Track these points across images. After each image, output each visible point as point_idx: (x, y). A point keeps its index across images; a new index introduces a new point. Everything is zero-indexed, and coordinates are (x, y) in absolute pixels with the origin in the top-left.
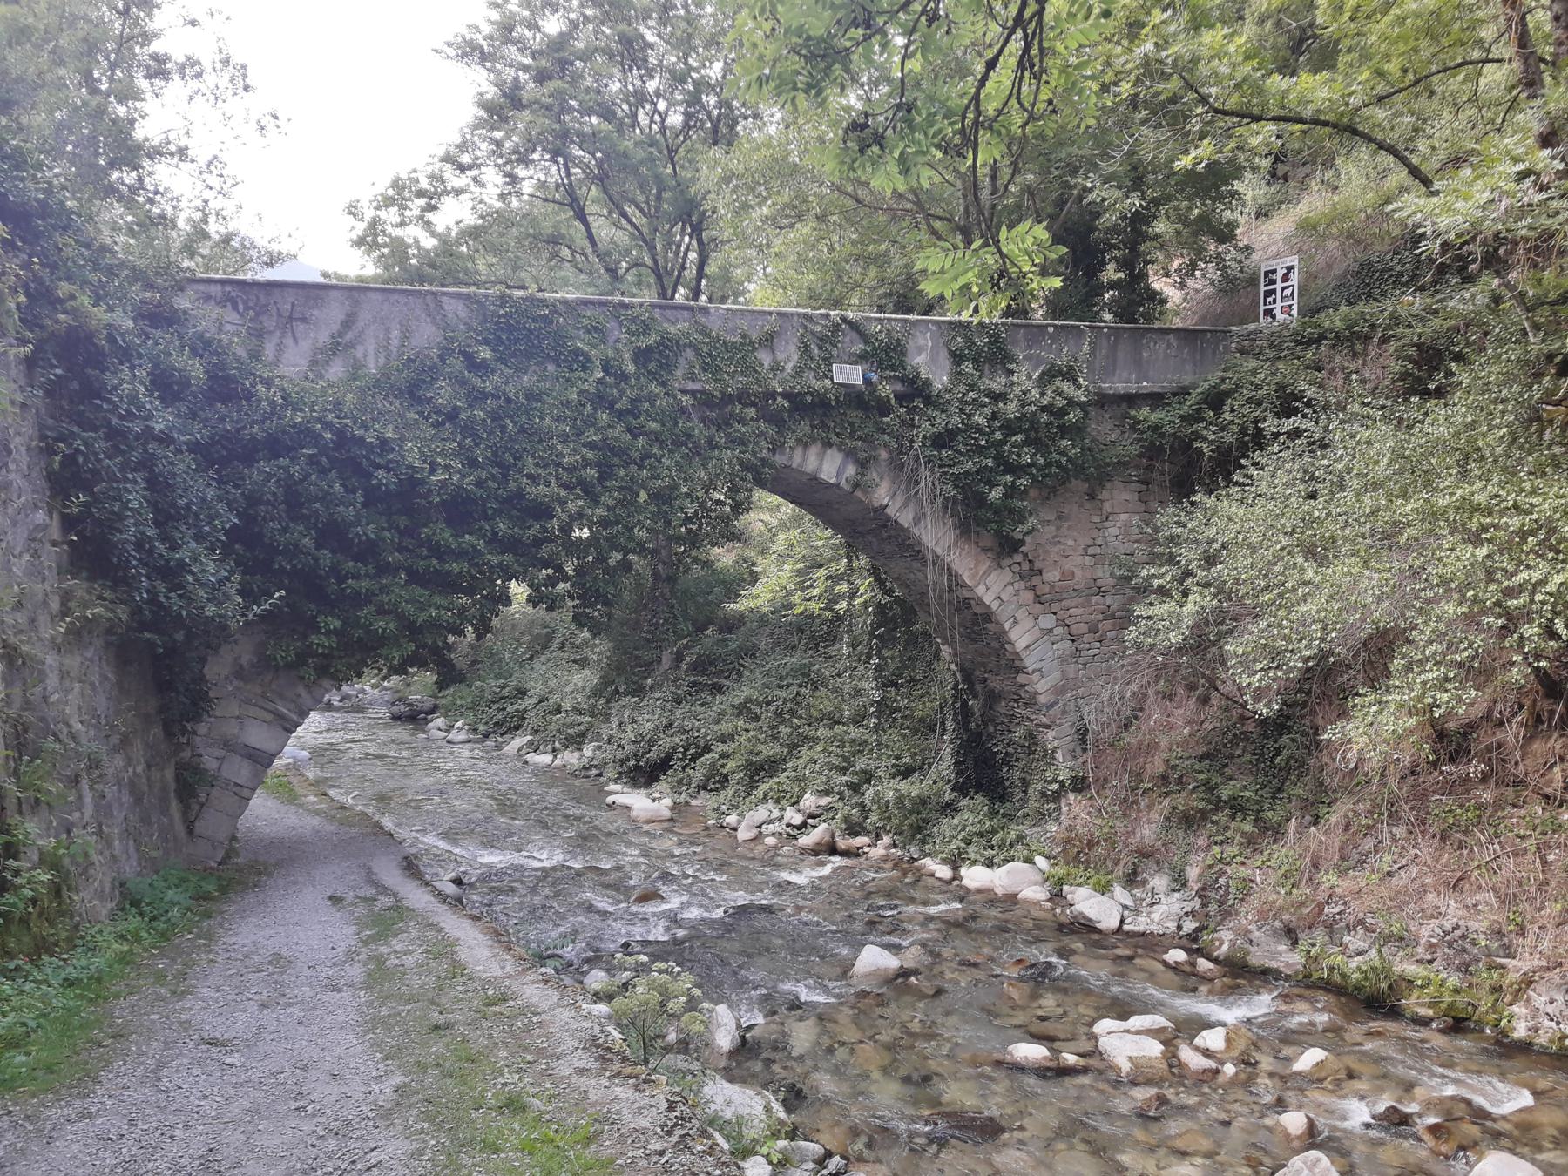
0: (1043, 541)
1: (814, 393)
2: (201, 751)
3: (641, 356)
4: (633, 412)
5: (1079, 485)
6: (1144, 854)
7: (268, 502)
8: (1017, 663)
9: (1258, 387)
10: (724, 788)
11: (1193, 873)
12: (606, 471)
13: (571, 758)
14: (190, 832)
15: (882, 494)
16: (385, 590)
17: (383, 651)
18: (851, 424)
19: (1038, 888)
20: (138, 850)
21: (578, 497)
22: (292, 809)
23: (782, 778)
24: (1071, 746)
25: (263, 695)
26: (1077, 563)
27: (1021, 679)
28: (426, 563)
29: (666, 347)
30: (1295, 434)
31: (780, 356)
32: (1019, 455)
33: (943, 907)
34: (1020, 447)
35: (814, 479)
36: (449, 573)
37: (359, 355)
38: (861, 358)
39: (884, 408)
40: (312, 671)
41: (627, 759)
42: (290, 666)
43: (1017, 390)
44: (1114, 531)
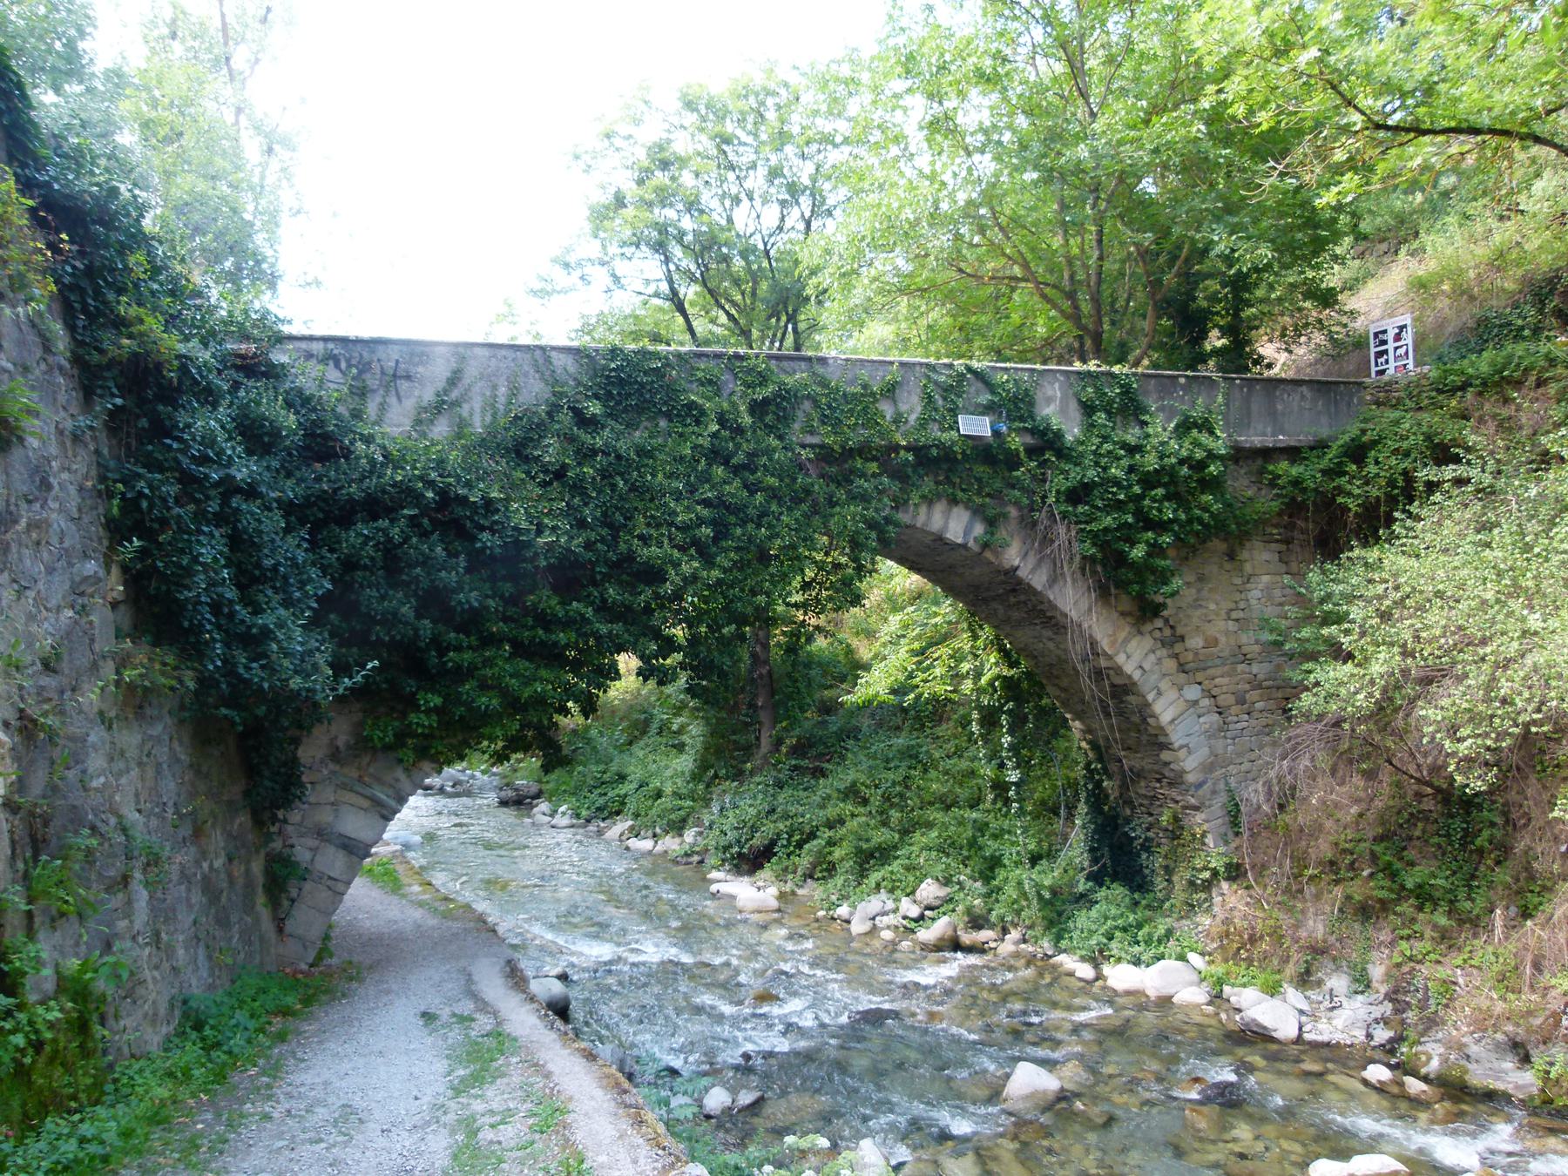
0: (1184, 605)
1: (940, 445)
2: (293, 841)
3: (758, 408)
4: (749, 467)
5: (1218, 545)
6: (1318, 950)
7: (365, 567)
8: (1162, 739)
9: (1404, 438)
10: (831, 876)
11: (1377, 972)
12: (721, 531)
13: (670, 844)
14: (280, 930)
15: (1013, 555)
16: (488, 662)
17: (486, 731)
18: (979, 480)
19: (1194, 989)
20: (210, 958)
21: (692, 558)
22: (395, 899)
23: (896, 866)
24: (1223, 830)
25: (360, 779)
26: (1219, 627)
27: (1165, 756)
28: (532, 633)
29: (784, 398)
30: (1460, 482)
31: (903, 408)
32: (1160, 511)
33: (1093, 1014)
34: (1160, 502)
35: (940, 539)
36: (555, 644)
37: (465, 414)
38: (988, 409)
39: (1013, 461)
40: (410, 753)
41: (730, 846)
42: (387, 748)
43: (1155, 441)
44: (1256, 593)
